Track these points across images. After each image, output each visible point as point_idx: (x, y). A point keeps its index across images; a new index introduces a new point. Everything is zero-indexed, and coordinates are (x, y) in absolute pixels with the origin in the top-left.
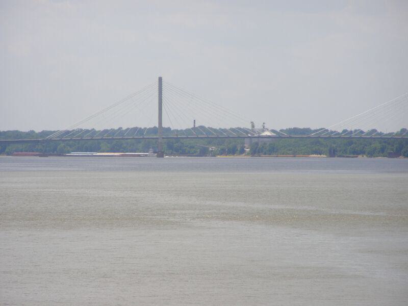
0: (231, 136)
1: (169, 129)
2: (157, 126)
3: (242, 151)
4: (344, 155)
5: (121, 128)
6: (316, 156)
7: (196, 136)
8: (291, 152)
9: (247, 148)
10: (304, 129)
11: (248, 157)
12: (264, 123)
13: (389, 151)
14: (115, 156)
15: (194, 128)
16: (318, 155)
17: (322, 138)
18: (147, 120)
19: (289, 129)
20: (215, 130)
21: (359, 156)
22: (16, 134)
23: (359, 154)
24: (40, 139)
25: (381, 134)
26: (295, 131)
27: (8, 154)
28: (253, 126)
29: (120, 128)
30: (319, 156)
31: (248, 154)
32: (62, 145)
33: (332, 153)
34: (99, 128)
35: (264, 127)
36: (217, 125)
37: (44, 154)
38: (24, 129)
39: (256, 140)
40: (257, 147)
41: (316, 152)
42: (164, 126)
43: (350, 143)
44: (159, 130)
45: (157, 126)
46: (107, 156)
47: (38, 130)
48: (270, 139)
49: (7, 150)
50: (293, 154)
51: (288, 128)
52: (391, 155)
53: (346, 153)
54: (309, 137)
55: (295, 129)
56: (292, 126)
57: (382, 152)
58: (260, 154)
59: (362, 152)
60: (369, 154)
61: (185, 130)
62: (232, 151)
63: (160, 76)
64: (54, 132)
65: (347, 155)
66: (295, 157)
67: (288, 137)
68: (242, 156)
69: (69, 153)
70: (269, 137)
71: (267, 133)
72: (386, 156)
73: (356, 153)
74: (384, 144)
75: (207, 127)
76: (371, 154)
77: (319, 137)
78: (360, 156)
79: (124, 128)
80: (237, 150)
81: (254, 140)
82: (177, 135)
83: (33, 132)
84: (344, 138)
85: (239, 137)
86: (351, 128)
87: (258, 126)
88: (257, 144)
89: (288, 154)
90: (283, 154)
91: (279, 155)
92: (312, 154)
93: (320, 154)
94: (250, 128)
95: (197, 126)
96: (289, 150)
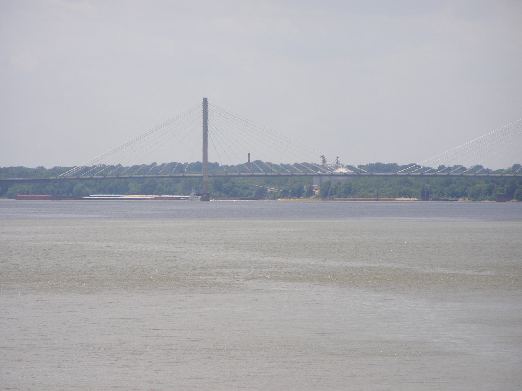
3: (310, 193)
4: (440, 198)
5: (155, 163)
6: (405, 199)
9: (317, 190)
12: (338, 158)
13: (498, 193)
16: (407, 198)
21: (459, 199)
22: (21, 171)
23: (459, 197)
24: (51, 178)
26: (378, 167)
28: (324, 161)
30: (408, 199)
31: (317, 197)
32: (80, 185)
33: (425, 195)
35: (337, 162)
36: (277, 161)
37: (56, 196)
38: (31, 164)
39: (328, 179)
41: (404, 195)
42: (251, 161)
43: (449, 183)
48: (346, 178)
50: (375, 197)
52: (500, 198)
53: (443, 195)
58: (333, 196)
59: (464, 195)
60: (472, 196)
62: (297, 193)
64: (70, 168)
70: (345, 175)
73: (455, 195)
76: (475, 197)
78: (461, 200)
81: (326, 179)
83: (42, 168)
87: (330, 161)
89: (370, 197)
94: (320, 163)
95: (252, 160)
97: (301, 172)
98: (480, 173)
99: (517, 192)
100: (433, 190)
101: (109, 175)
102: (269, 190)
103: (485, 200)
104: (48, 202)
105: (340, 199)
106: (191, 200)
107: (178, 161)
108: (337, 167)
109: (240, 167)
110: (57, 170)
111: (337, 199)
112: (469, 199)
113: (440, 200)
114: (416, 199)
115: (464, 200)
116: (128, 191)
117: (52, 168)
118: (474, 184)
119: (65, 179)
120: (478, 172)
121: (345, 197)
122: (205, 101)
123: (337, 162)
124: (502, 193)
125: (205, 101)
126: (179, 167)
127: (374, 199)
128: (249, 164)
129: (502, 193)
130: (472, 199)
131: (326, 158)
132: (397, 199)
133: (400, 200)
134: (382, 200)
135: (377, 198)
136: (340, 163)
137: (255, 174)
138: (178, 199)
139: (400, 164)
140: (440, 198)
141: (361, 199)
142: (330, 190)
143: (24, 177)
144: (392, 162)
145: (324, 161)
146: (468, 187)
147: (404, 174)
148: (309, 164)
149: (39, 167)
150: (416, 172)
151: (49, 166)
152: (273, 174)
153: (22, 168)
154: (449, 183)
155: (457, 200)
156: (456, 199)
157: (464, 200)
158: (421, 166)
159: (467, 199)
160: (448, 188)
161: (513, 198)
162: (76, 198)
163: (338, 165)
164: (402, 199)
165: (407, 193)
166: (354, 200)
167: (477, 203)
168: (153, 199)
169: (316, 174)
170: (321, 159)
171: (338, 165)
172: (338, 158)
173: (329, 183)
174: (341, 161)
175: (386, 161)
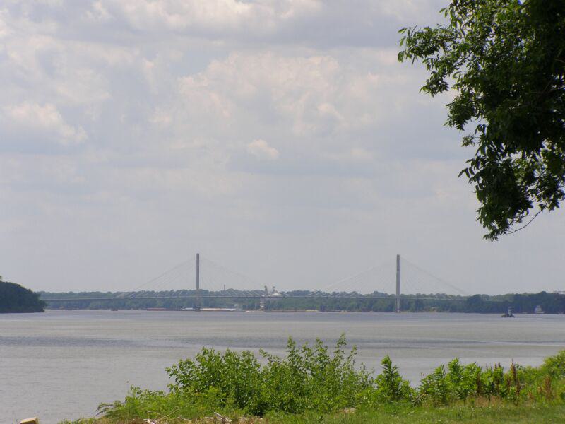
3: (258, 307)
22: (98, 295)
26: (298, 293)
27: (91, 309)
28: (266, 290)
33: (323, 309)
36: (241, 288)
38: (104, 290)
41: (311, 308)
42: (200, 288)
52: (364, 310)
59: (344, 308)
62: (251, 308)
70: (276, 297)
71: (276, 294)
73: (339, 309)
76: (350, 310)
78: (343, 311)
81: (267, 299)
94: (264, 289)
107: (22, 285)
108: (273, 293)
110: (118, 294)
117: (389, 294)
119: (119, 299)
122: (198, 255)
125: (198, 255)
128: (224, 292)
131: (428, 80)
135: (296, 310)
139: (311, 291)
144: (307, 290)
145: (266, 290)
151: (113, 292)
153: (98, 292)
163: (274, 292)
167: (351, 313)
173: (269, 302)
174: (276, 290)
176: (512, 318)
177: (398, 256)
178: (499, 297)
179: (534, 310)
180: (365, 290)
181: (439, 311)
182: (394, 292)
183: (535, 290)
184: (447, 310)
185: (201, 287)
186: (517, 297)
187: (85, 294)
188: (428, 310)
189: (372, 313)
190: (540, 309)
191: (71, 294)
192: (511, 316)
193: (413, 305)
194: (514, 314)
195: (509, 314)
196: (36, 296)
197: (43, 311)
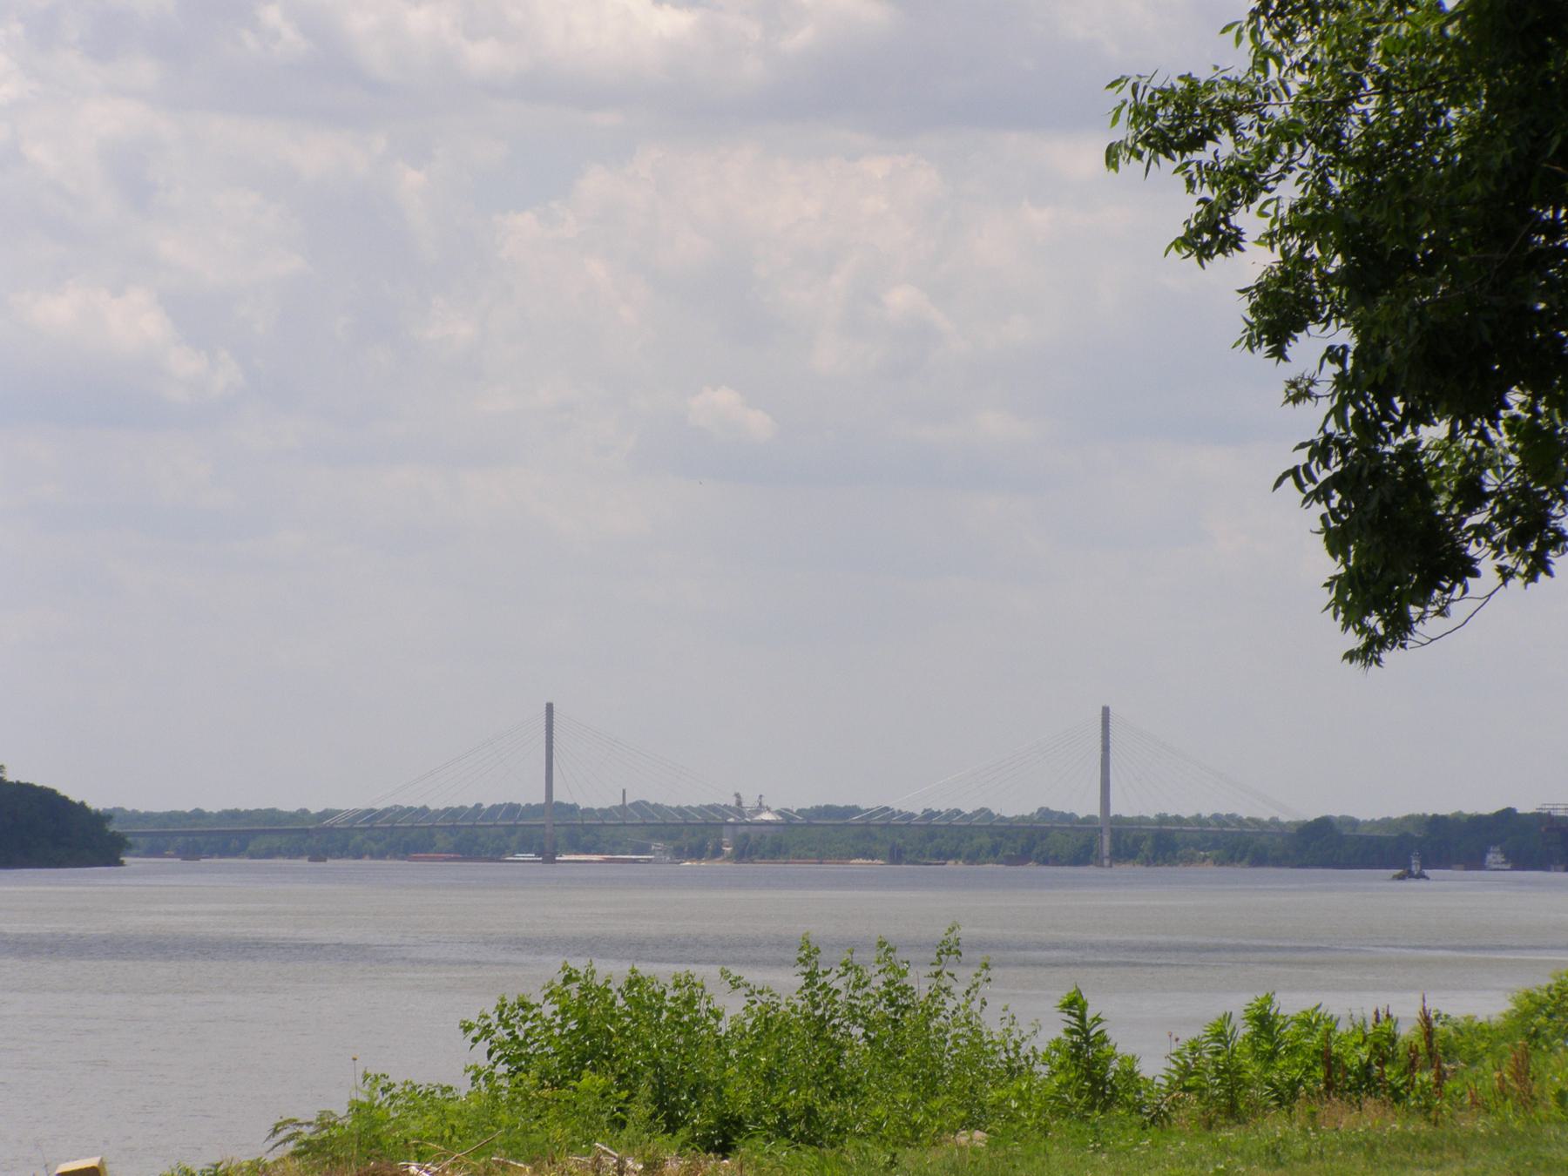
0: (691, 821)
1: (573, 809)
2: (1098, 814)
3: (717, 853)
4: (919, 860)
5: (481, 805)
6: (865, 861)
7: (621, 822)
8: (813, 854)
9: (728, 847)
10: (846, 807)
11: (728, 864)
12: (761, 796)
13: (1007, 853)
14: (591, 861)
15: (623, 806)
16: (867, 859)
17: (876, 825)
18: (1085, 805)
19: (817, 807)
20: (1240, 821)
21: (949, 862)
22: (272, 816)
23: (948, 858)
24: (310, 827)
25: (1003, 819)
26: (828, 811)
27: (252, 856)
28: (739, 803)
29: (478, 806)
30: (870, 861)
31: (728, 859)
32: (359, 838)
33: (896, 856)
34: (436, 803)
35: (760, 804)
36: (671, 801)
37: (318, 856)
38: (289, 805)
39: (745, 829)
40: (747, 844)
41: (865, 854)
42: (556, 799)
43: (932, 837)
44: (553, 808)
45: (1098, 814)
46: (586, 862)
47: (315, 809)
48: (773, 828)
49: (251, 848)
50: (817, 859)
51: (814, 805)
52: (1010, 861)
53: (924, 856)
54: (846, 825)
55: (827, 807)
56: (823, 802)
57: (994, 853)
58: (753, 857)
59: (954, 855)
60: (968, 857)
61: (61, 797)
62: (697, 853)
63: (549, 701)
64: (340, 812)
65: (791, 860)
66: (821, 863)
67: (803, 825)
68: (717, 864)
69: (513, 855)
70: (768, 823)
71: (767, 816)
72: (1002, 863)
73: (942, 856)
74: (998, 839)
75: (1245, 817)
76: (973, 858)
77: (867, 825)
78: (951, 863)
79: (486, 805)
80: (707, 849)
81: (742, 830)
82: (582, 820)
83: (304, 812)
84: (919, 826)
85: (707, 824)
86: (941, 805)
87: (749, 802)
88: (746, 837)
89: (810, 858)
90: (799, 858)
91: (791, 860)
92: (857, 857)
93: (873, 859)
94: (733, 803)
95: (629, 801)
96: (811, 850)
97: (680, 819)
98: (978, 821)
99: (1036, 851)
100: (909, 848)
101: (400, 823)
102: (653, 847)
103: (988, 863)
104: (215, 861)
105: (763, 861)
106: (655, 863)
107: (63, 791)
109: (605, 813)
111: (759, 861)
112: (964, 862)
113: (919, 864)
114: (882, 862)
115: (956, 863)
116: (434, 848)
118: (972, 839)
120: (877, 818)
121: (772, 858)
122: (550, 707)
123: (760, 804)
124: (1013, 853)
125: (550, 707)
126: (512, 809)
127: (816, 861)
129: (1013, 853)
130: (968, 861)
132: (852, 862)
133: (856, 864)
134: (828, 863)
136: (765, 804)
137: (606, 822)
138: (635, 861)
140: (919, 860)
141: (797, 861)
142: (748, 847)
143: (275, 825)
144: (851, 804)
146: (962, 844)
147: (860, 822)
148: (1358, 820)
149: (301, 810)
150: (879, 819)
152: (655, 821)
153: (273, 811)
154: (932, 837)
155: (943, 864)
156: (943, 862)
157: (956, 863)
158: (943, 810)
159: (960, 862)
160: (930, 845)
161: (1030, 860)
162: (491, 860)
163: (760, 808)
164: (861, 861)
165: (868, 853)
166: (785, 863)
168: (600, 862)
169: (742, 821)
170: (735, 799)
171: (760, 808)
172: (761, 796)
175: (840, 802)
176: (1422, 883)
177: (1106, 712)
178: (1386, 823)
179: (1483, 858)
180: (1014, 804)
181: (1219, 862)
182: (538, 798)
183: (1487, 805)
184: (1241, 859)
185: (556, 799)
186: (1436, 823)
187: (234, 815)
188: (1190, 861)
189: (1032, 868)
190: (1500, 858)
191: (199, 814)
192: (1421, 876)
193: (1146, 846)
194: (1427, 872)
195: (1415, 869)
196: (100, 820)
197: (121, 864)
